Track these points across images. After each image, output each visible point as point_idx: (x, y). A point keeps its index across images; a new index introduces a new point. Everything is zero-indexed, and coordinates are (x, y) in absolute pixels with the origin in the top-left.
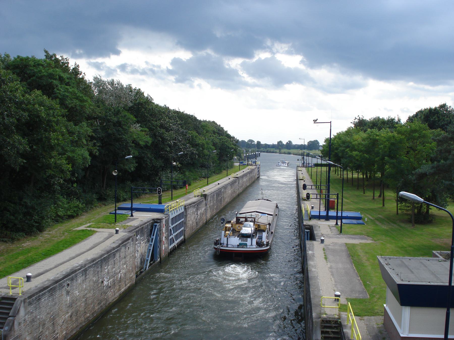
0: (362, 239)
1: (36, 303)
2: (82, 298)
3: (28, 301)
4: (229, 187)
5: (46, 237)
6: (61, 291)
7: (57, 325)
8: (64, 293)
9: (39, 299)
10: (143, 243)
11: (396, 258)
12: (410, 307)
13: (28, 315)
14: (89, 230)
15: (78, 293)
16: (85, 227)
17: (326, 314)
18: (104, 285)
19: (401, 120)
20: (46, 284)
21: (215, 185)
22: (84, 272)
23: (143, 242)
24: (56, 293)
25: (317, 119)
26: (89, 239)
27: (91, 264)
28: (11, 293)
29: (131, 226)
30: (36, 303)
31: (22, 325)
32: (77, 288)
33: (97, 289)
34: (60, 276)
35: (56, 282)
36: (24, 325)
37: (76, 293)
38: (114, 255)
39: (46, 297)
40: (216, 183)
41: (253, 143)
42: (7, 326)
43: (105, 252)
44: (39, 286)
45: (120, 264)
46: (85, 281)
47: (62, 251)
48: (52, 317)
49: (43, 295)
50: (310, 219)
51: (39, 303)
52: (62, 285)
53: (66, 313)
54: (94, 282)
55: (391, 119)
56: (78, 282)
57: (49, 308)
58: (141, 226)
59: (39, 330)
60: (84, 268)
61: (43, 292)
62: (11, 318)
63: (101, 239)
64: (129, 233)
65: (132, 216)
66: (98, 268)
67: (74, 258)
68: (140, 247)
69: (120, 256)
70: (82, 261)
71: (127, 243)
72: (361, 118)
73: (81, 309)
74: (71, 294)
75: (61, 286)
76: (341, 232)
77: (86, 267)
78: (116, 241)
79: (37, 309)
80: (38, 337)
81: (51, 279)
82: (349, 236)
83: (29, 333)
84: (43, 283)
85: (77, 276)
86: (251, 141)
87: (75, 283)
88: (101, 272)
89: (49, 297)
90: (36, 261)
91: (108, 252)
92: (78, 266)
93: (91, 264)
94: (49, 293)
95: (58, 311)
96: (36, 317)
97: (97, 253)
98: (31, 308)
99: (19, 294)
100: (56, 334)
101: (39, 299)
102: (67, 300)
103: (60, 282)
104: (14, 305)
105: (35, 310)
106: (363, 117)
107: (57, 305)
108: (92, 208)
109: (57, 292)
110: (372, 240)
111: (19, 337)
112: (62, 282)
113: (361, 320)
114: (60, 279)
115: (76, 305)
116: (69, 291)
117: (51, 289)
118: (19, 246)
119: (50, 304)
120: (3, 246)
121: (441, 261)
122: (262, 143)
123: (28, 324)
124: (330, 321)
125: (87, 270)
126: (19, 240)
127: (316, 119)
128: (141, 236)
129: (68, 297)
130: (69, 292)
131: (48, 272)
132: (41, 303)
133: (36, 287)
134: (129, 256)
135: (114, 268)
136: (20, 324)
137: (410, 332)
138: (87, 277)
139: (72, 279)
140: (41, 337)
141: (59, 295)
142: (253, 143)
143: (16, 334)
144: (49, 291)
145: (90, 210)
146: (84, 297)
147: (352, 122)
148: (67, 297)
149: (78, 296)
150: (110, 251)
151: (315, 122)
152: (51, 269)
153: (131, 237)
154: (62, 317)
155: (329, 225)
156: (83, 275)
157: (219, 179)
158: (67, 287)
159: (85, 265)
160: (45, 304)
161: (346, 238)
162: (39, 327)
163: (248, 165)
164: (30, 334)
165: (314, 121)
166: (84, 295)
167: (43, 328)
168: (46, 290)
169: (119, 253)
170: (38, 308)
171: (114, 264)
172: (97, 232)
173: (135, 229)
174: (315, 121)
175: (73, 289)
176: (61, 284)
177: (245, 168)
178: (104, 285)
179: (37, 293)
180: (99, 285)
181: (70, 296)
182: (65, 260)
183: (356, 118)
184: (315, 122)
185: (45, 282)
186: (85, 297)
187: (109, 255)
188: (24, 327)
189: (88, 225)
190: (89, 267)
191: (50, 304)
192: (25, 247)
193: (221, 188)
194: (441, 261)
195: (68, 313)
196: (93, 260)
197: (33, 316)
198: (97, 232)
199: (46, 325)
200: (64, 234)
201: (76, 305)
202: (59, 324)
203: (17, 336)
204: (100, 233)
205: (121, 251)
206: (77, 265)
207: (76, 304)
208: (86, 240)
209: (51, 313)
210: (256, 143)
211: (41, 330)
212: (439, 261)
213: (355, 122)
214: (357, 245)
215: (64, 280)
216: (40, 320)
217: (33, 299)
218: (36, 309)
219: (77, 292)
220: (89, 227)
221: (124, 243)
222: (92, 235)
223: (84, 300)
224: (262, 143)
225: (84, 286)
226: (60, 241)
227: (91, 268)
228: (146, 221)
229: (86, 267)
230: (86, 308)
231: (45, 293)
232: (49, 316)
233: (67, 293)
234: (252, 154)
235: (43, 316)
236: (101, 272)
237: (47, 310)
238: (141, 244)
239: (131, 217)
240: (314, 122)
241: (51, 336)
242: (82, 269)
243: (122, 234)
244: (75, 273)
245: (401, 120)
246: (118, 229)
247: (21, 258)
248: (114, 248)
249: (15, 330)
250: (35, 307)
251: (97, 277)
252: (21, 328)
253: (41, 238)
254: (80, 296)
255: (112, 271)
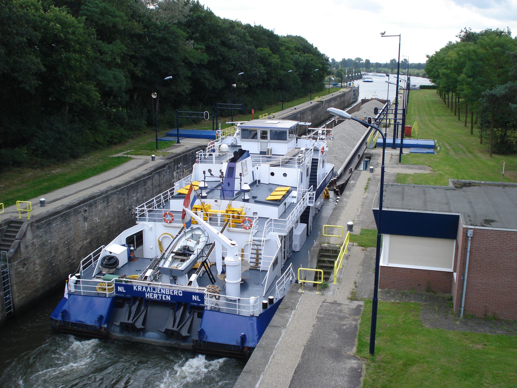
0: (420, 169)
1: (45, 227)
2: (104, 225)
3: (35, 225)
4: (309, 113)
5: (79, 164)
6: (76, 216)
7: (74, 251)
8: (81, 219)
9: (49, 223)
10: (188, 171)
11: (400, 185)
12: (389, 235)
13: (37, 239)
14: (124, 157)
15: (98, 220)
16: (123, 154)
17: (328, 243)
18: (133, 213)
19: (511, 33)
20: (58, 209)
21: (290, 110)
22: (105, 198)
23: (187, 171)
24: (71, 218)
25: (385, 32)
26: (122, 166)
27: (115, 191)
28: (20, 216)
29: (172, 153)
30: (45, 227)
31: (30, 248)
32: (97, 215)
33: (123, 217)
34: (76, 202)
35: (70, 207)
36: (32, 249)
37: (96, 220)
38: (145, 182)
39: (58, 222)
40: (293, 108)
41: (361, 62)
42: (13, 248)
43: (133, 179)
44: (50, 211)
45: (153, 192)
46: (108, 208)
47: (89, 178)
48: (66, 242)
49: (54, 219)
50: (375, 147)
51: (50, 228)
52: (78, 211)
53: (85, 239)
54: (120, 210)
55: (500, 32)
56: (98, 208)
57: (63, 233)
58: (183, 153)
59: (51, 255)
60: (105, 194)
61: (54, 217)
62: (17, 241)
63: (134, 167)
64: (166, 160)
65: (178, 142)
66: (124, 195)
67: (98, 184)
68: (183, 175)
69: (153, 184)
70: (105, 188)
71: (162, 171)
72: (468, 30)
73: (103, 236)
74: (90, 220)
75: (77, 212)
76: (400, 161)
77: (109, 193)
78: (149, 168)
79: (47, 234)
80: (49, 261)
81: (66, 204)
82: (407, 165)
83: (39, 256)
84: (55, 208)
85: (97, 203)
86: (359, 59)
87: (94, 209)
88: (128, 200)
89: (62, 222)
90: (58, 187)
91: (136, 179)
92: (98, 193)
93: (115, 191)
94: (61, 218)
95: (73, 237)
96: (46, 241)
97: (124, 180)
98: (40, 232)
99: (28, 218)
100: (71, 259)
101: (50, 223)
102: (85, 226)
103: (75, 208)
104: (21, 229)
105: (44, 234)
106: (471, 29)
107: (72, 230)
108: (140, 134)
109: (72, 217)
110: (431, 170)
111: (27, 259)
112: (78, 207)
113: (363, 250)
114: (74, 205)
115: (96, 232)
116: (86, 217)
117: (64, 214)
118: (47, 173)
119: (63, 229)
120: (31, 173)
121: (448, 190)
122: (372, 61)
123: (38, 248)
124: (329, 250)
125: (110, 197)
126: (48, 166)
127: (384, 32)
128: (184, 164)
129: (86, 224)
130: (87, 218)
131: (65, 198)
132: (51, 228)
133: (48, 211)
134: (165, 184)
135: (146, 196)
136: (27, 247)
137: (389, 262)
138: (110, 203)
139: (90, 206)
140: (53, 261)
141: (74, 220)
142: (361, 62)
143: (23, 256)
144: (61, 216)
145: (137, 136)
146: (106, 224)
147: (458, 35)
148: (84, 223)
149: (99, 223)
150: (138, 178)
151: (383, 35)
152: (70, 195)
153: (167, 164)
154: (79, 243)
155: (392, 154)
156: (104, 202)
157: (297, 105)
158: (85, 213)
159: (107, 192)
160: (57, 228)
161: (402, 168)
162: (51, 251)
163: (342, 87)
164: (40, 257)
165: (381, 34)
166: (106, 223)
167: (55, 253)
168: (58, 215)
169: (151, 181)
170: (49, 232)
171: (145, 192)
172: (133, 159)
173: (176, 156)
174: (383, 34)
175: (92, 216)
176: (76, 209)
177: (337, 91)
178: (132, 212)
179: (46, 217)
180: (126, 213)
181: (89, 222)
182: (88, 187)
183: (462, 30)
184: (383, 35)
185: (59, 207)
186: (108, 224)
187: (138, 182)
188: (32, 251)
189: (126, 152)
190: (111, 194)
191: (63, 229)
192: (54, 173)
193: (296, 113)
194: (448, 190)
195: (86, 239)
196: (117, 187)
197: (43, 240)
198: (133, 159)
199: (59, 250)
200: (98, 161)
201: (96, 232)
202: (75, 250)
203: (24, 259)
204: (135, 160)
205: (154, 178)
206: (98, 191)
207: (97, 231)
208: (118, 167)
209: (65, 238)
210: (364, 62)
211: (53, 254)
212: (447, 190)
213: (460, 35)
214: (410, 175)
215: (80, 205)
216: (52, 244)
217: (42, 223)
218: (46, 233)
219: (97, 219)
220: (127, 154)
221: (158, 170)
222: (127, 162)
223: (106, 227)
224: (371, 62)
225: (107, 213)
226: (91, 167)
227: (114, 195)
228: (191, 148)
229: (109, 193)
230: (109, 236)
231: (56, 218)
232: (63, 241)
233: (84, 219)
234: (356, 74)
235: (55, 240)
236: (128, 199)
237: (59, 235)
238: (184, 173)
239: (177, 144)
240: (381, 35)
241: (66, 261)
242: (103, 196)
243: (159, 160)
244: (94, 200)
245: (511, 33)
246: (153, 155)
247: (46, 184)
248: (144, 176)
249: (22, 252)
250: (45, 231)
251: (123, 205)
252: (28, 251)
253: (73, 165)
254: (101, 223)
255: (143, 199)
